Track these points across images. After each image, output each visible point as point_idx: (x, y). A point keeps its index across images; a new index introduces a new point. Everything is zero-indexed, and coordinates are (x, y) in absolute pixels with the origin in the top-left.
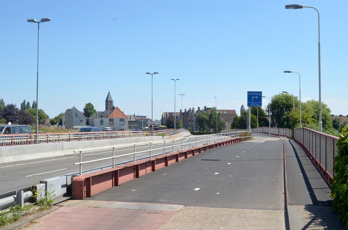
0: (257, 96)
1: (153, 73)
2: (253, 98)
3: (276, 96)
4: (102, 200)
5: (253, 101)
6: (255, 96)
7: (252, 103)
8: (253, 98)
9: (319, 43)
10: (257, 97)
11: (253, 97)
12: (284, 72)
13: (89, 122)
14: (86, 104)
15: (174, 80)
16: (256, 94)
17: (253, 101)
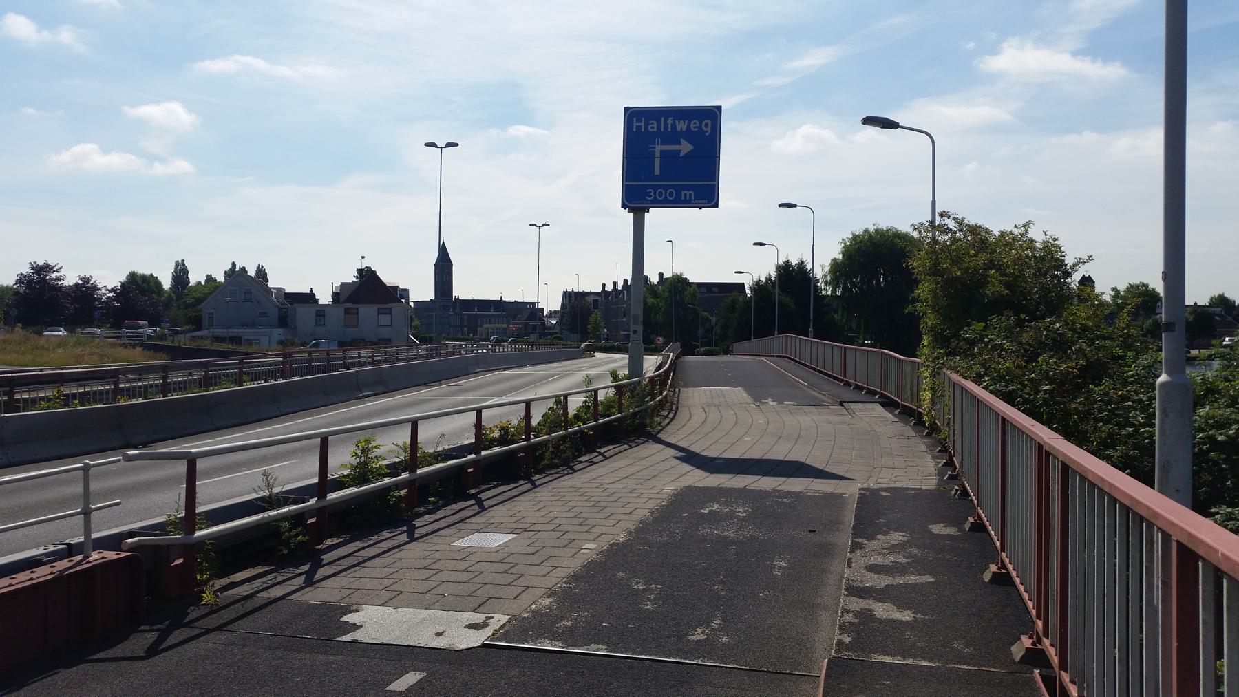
0: (689, 135)
1: (444, 146)
2: (658, 154)
4: (383, 644)
5: (657, 172)
6: (673, 137)
7: (655, 188)
8: (658, 154)
10: (685, 147)
11: (659, 149)
12: (754, 244)
13: (288, 319)
16: (681, 126)
17: (657, 172)
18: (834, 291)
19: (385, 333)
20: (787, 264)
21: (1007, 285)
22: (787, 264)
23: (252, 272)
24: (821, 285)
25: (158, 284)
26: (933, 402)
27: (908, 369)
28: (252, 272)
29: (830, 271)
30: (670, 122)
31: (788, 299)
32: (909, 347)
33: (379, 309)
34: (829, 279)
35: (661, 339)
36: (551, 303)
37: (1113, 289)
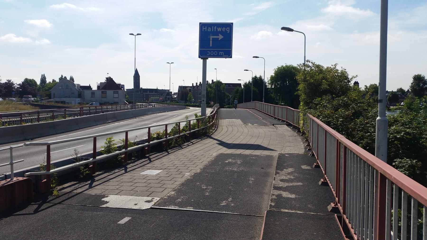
0: (221, 33)
3: (279, 68)
5: (211, 45)
6: (217, 33)
7: (210, 51)
9: (264, 71)
10: (221, 37)
11: (211, 37)
14: (106, 78)
15: (169, 63)
16: (219, 29)
17: (211, 45)
18: (271, 86)
19: (116, 100)
20: (256, 77)
21: (329, 85)
22: (256, 77)
23: (68, 79)
24: (267, 84)
25: (35, 83)
26: (304, 124)
27: (295, 113)
28: (68, 79)
29: (270, 80)
30: (215, 28)
31: (256, 89)
32: (296, 106)
33: (114, 92)
34: (270, 82)
35: (213, 103)
36: (175, 90)
37: (365, 86)
